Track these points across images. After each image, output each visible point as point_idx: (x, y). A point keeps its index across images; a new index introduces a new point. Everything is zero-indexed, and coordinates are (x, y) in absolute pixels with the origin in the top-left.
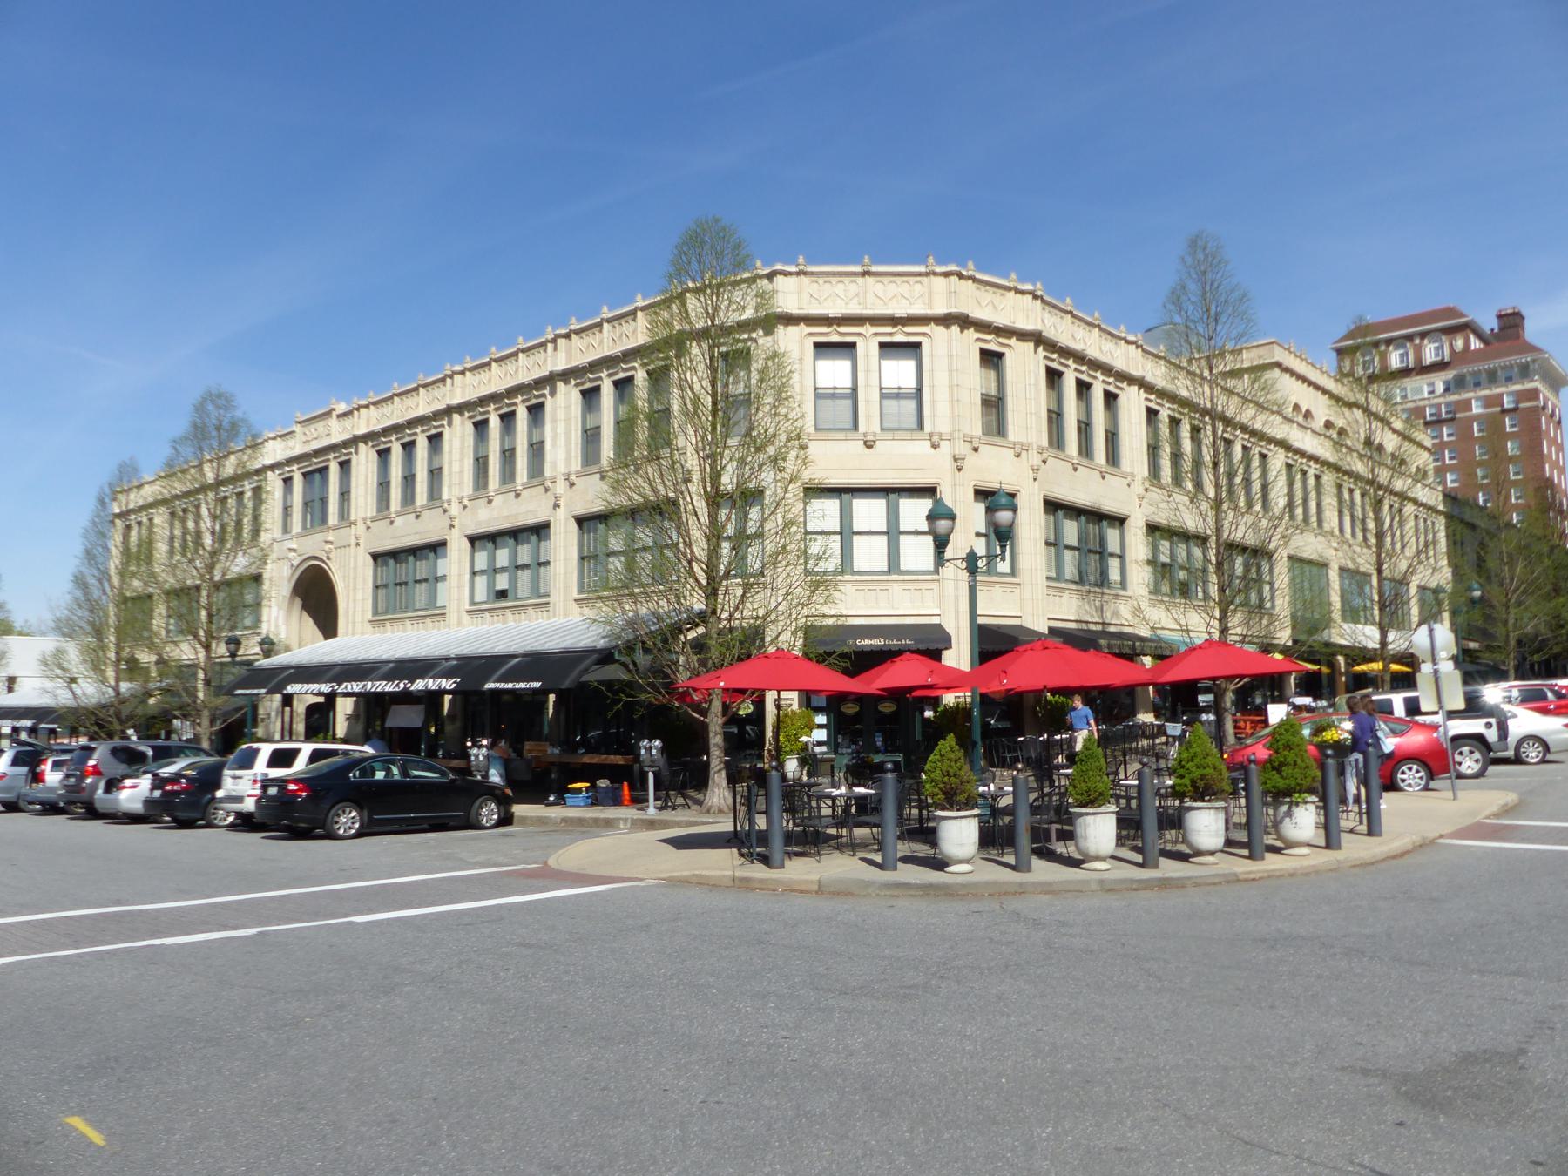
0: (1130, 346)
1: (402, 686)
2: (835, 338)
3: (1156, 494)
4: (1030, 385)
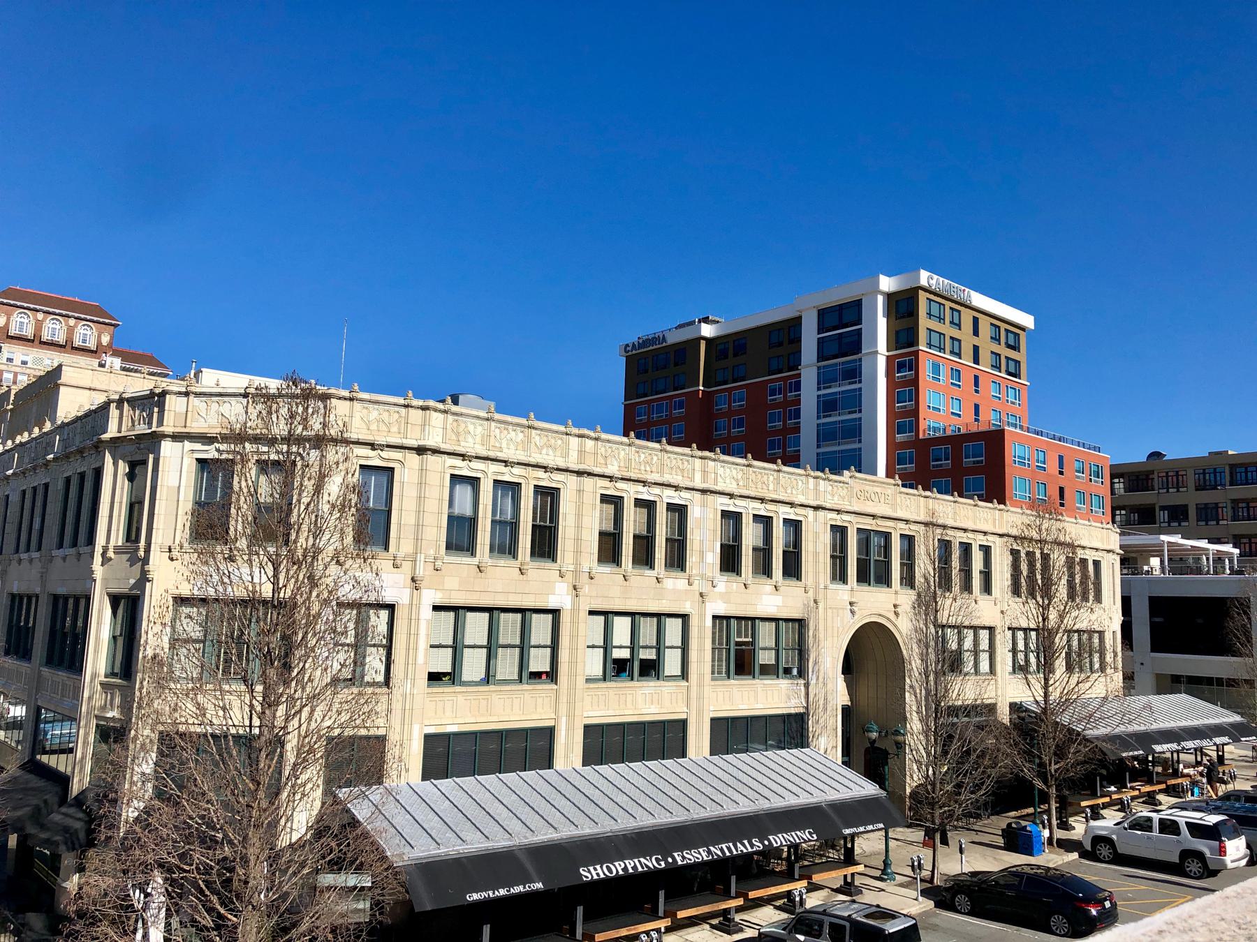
3: (725, 582)
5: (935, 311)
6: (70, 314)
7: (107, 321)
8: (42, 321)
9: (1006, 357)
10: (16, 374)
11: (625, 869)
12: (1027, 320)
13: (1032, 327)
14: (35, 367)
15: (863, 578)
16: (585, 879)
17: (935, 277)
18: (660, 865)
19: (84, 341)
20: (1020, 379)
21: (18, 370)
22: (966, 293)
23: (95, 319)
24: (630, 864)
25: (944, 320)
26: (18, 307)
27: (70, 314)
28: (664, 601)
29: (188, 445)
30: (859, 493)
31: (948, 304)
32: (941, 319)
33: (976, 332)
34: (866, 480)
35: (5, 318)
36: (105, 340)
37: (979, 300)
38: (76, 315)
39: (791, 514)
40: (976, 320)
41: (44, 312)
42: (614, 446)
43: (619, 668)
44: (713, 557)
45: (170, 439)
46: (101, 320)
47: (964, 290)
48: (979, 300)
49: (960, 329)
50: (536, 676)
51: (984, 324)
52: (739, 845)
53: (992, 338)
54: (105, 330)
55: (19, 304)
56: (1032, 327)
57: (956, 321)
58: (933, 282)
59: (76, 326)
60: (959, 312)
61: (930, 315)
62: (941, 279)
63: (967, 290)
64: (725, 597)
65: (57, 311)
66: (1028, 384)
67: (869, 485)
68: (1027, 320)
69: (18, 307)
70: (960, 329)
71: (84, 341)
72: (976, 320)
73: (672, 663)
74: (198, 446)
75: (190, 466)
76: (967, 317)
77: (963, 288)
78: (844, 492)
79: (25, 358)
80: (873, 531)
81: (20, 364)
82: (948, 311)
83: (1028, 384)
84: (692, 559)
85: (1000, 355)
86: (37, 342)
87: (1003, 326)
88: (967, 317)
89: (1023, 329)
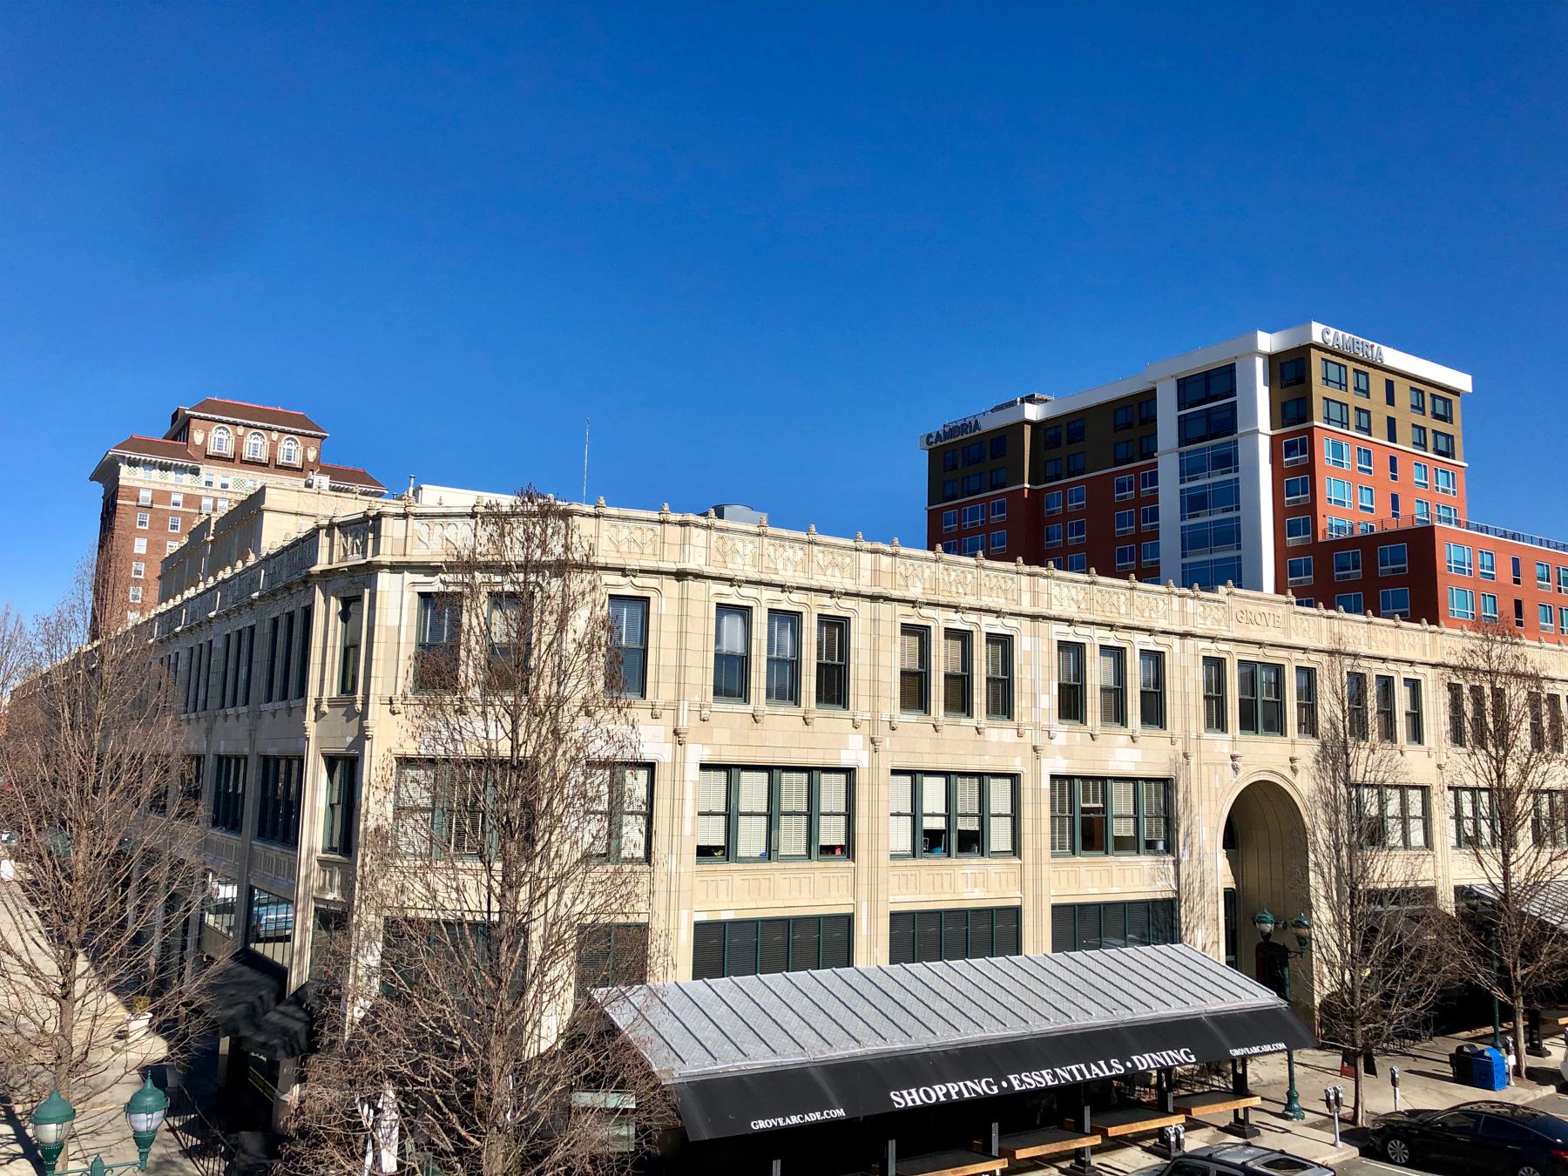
3: (1064, 733)
5: (1334, 375)
6: (273, 426)
7: (313, 433)
8: (242, 436)
9: (1434, 431)
10: (216, 500)
11: (948, 1094)
12: (1461, 381)
13: (1470, 390)
14: (236, 490)
15: (1248, 723)
16: (897, 1106)
17: (1333, 331)
18: (992, 1090)
19: (289, 458)
20: (1454, 458)
21: (217, 494)
22: (1375, 349)
23: (300, 431)
24: (953, 1088)
25: (1346, 385)
26: (216, 421)
27: (273, 426)
28: (987, 757)
29: (409, 577)
30: (1240, 614)
31: (1351, 365)
32: (1342, 385)
33: (1390, 400)
34: (1248, 597)
35: (203, 435)
36: (312, 455)
37: (1394, 358)
38: (280, 427)
39: (1151, 643)
40: (1390, 385)
41: (279, 431)
43: (932, 842)
44: (1049, 700)
45: (388, 570)
46: (307, 432)
47: (1372, 346)
48: (1394, 358)
49: (1368, 397)
50: (828, 850)
51: (1402, 390)
52: (1093, 1067)
53: (1412, 406)
54: (311, 443)
55: (217, 417)
56: (1470, 390)
57: (1363, 386)
58: (1330, 337)
59: (279, 440)
60: (1366, 374)
61: (1326, 380)
62: (1341, 333)
63: (1376, 345)
64: (1067, 752)
65: (259, 424)
66: (1466, 465)
67: (1254, 604)
68: (1461, 381)
69: (216, 421)
70: (1368, 397)
71: (289, 458)
72: (1390, 385)
73: (999, 834)
74: (420, 578)
75: (411, 602)
76: (1377, 381)
77: (1371, 343)
78: (1219, 614)
79: (225, 481)
80: (1259, 663)
81: (219, 488)
82: (1351, 374)
83: (1466, 465)
84: (1021, 703)
85: (1424, 429)
86: (272, 467)
87: (1428, 390)
88: (1377, 381)
89: (1456, 393)
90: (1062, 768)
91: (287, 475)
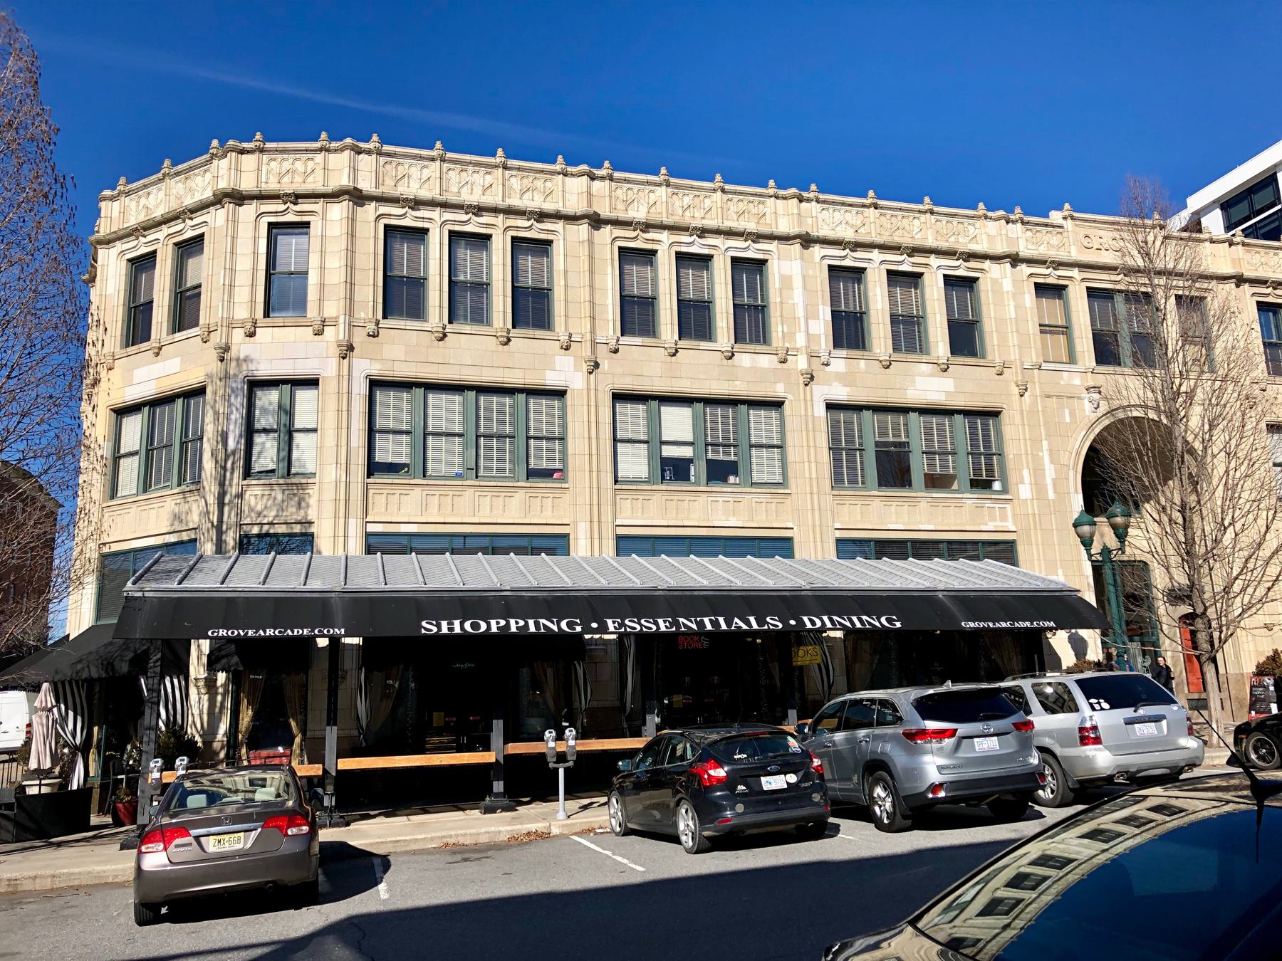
0: (789, 201)
1: (236, 633)
2: (848, 263)
3: (841, 362)
4: (584, 271)
42: (636, 187)
64: (844, 379)
78: (1055, 240)
80: (1120, 291)
90: (841, 394)
91: (770, 333)
